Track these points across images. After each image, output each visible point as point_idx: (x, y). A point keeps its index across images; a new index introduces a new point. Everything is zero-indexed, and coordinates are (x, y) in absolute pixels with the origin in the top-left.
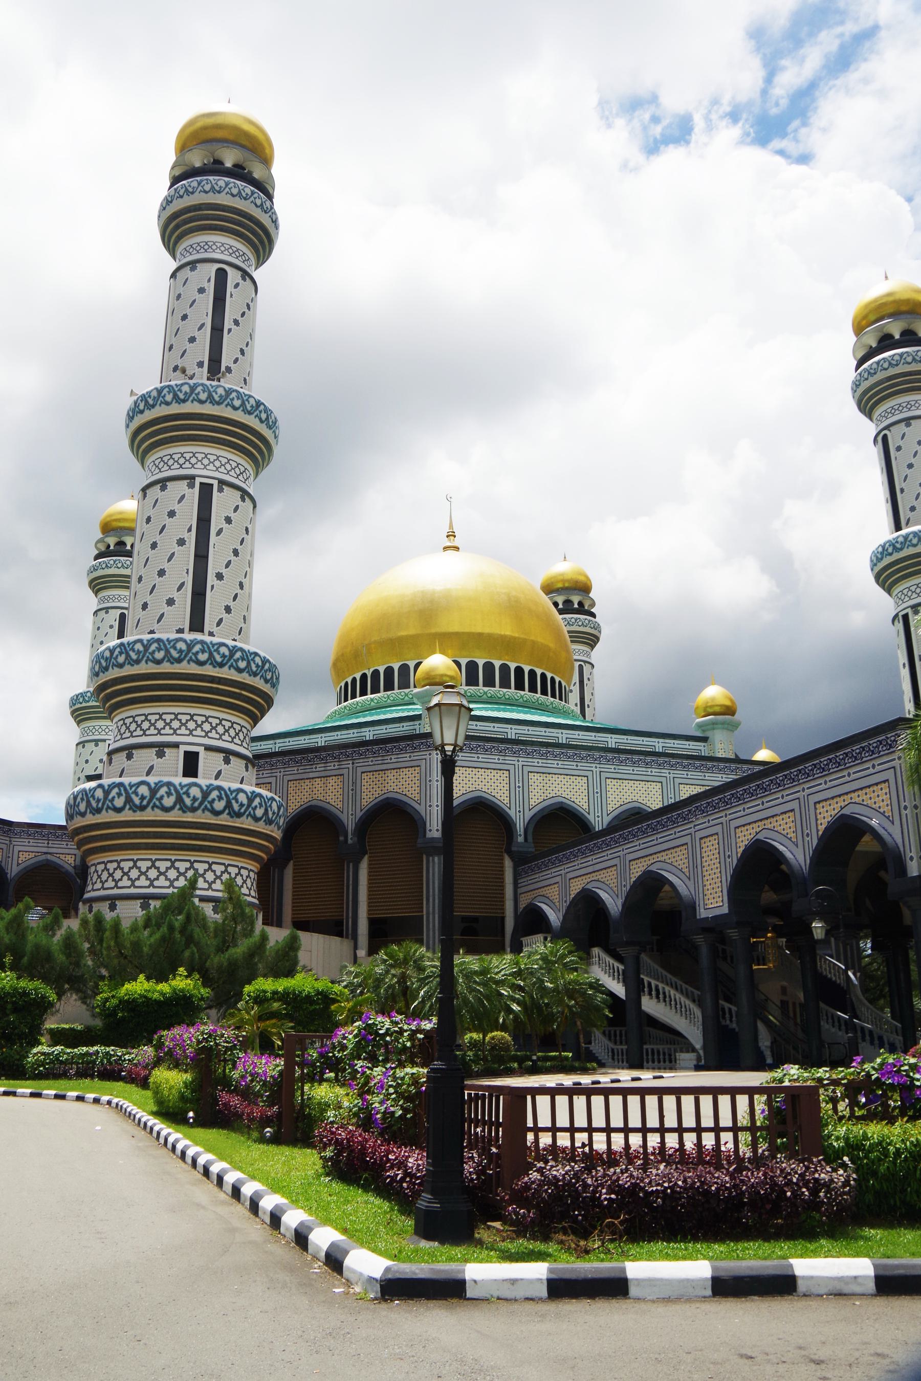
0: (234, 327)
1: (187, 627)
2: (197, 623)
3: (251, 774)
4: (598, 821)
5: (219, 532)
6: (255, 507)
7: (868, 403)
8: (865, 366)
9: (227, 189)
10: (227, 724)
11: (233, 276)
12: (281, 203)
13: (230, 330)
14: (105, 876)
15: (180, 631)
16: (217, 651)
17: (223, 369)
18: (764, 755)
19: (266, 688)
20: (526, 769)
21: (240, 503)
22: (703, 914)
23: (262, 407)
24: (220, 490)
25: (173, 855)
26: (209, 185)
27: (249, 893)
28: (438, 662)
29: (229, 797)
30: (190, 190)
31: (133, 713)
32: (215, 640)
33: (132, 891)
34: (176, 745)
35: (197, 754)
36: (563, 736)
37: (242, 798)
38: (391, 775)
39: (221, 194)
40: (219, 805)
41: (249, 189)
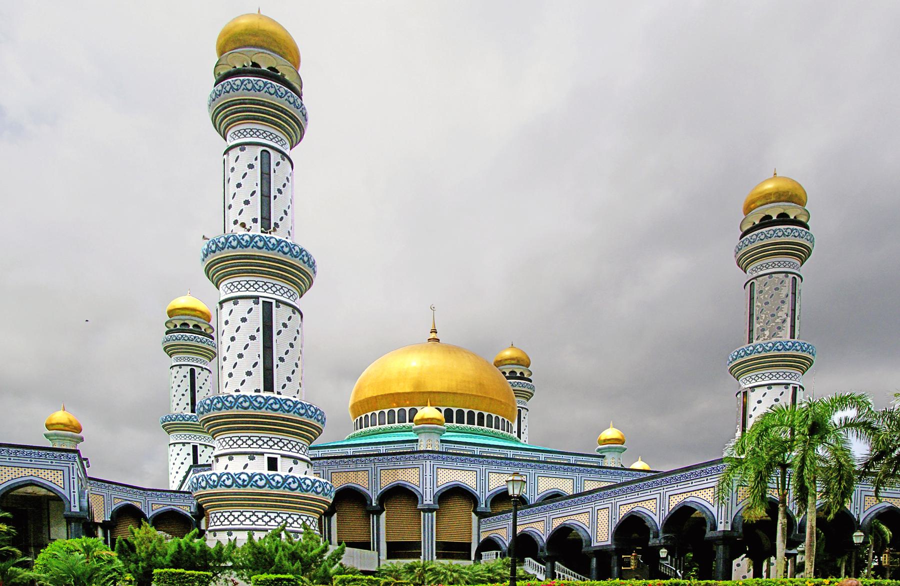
0: (278, 195)
1: (262, 389)
2: (269, 385)
3: (310, 471)
4: (532, 498)
5: (279, 333)
6: (302, 317)
7: (744, 261)
8: (748, 236)
9: (266, 89)
10: (294, 444)
11: (275, 157)
12: (308, 100)
13: (275, 197)
14: (215, 519)
15: (258, 391)
16: (285, 403)
17: (272, 226)
18: (639, 465)
19: (318, 424)
20: (487, 471)
21: (292, 315)
22: (595, 544)
23: (304, 253)
24: (278, 306)
25: (222, 510)
26: (251, 85)
27: (314, 528)
28: (428, 412)
29: (300, 482)
30: (235, 87)
31: (224, 436)
32: (283, 397)
33: (221, 527)
34: (262, 454)
35: (276, 459)
36: (510, 454)
37: (308, 482)
38: (400, 471)
39: (259, 89)
40: (203, 484)
41: (284, 89)
